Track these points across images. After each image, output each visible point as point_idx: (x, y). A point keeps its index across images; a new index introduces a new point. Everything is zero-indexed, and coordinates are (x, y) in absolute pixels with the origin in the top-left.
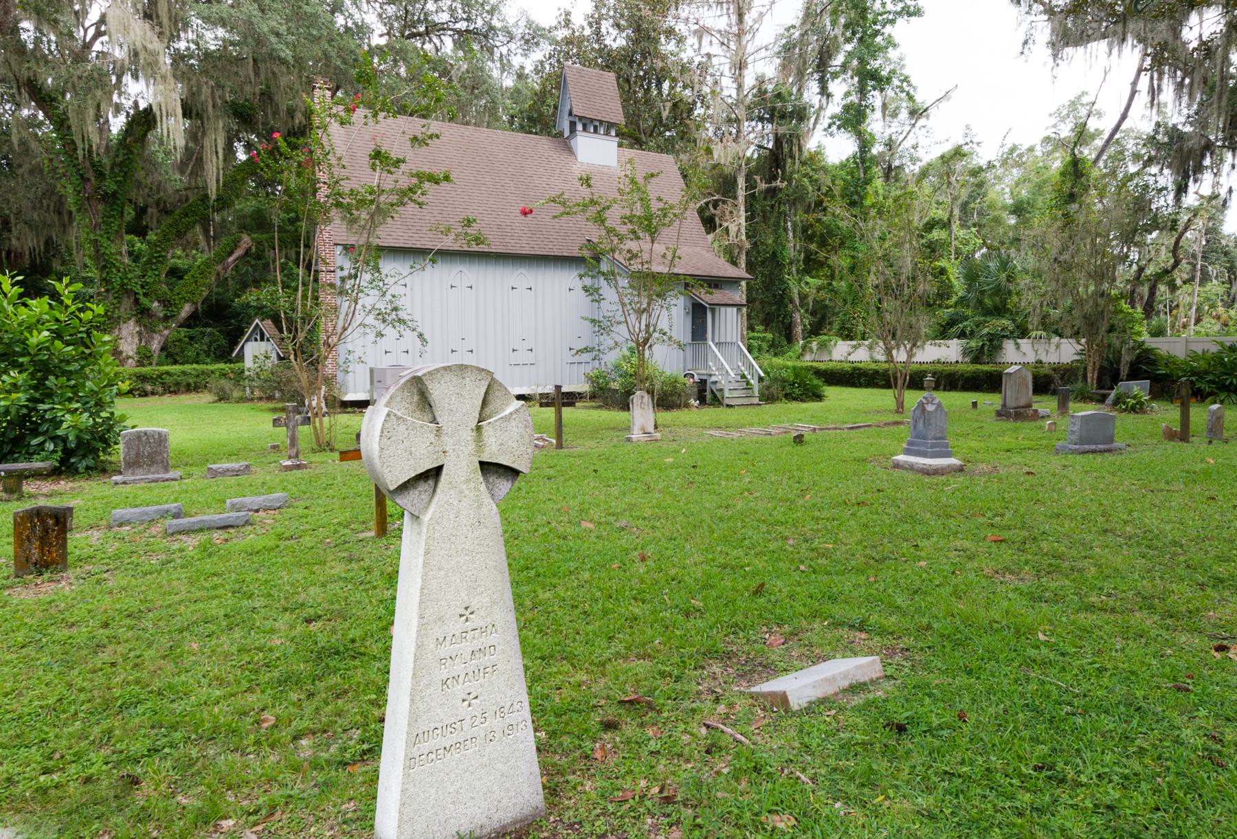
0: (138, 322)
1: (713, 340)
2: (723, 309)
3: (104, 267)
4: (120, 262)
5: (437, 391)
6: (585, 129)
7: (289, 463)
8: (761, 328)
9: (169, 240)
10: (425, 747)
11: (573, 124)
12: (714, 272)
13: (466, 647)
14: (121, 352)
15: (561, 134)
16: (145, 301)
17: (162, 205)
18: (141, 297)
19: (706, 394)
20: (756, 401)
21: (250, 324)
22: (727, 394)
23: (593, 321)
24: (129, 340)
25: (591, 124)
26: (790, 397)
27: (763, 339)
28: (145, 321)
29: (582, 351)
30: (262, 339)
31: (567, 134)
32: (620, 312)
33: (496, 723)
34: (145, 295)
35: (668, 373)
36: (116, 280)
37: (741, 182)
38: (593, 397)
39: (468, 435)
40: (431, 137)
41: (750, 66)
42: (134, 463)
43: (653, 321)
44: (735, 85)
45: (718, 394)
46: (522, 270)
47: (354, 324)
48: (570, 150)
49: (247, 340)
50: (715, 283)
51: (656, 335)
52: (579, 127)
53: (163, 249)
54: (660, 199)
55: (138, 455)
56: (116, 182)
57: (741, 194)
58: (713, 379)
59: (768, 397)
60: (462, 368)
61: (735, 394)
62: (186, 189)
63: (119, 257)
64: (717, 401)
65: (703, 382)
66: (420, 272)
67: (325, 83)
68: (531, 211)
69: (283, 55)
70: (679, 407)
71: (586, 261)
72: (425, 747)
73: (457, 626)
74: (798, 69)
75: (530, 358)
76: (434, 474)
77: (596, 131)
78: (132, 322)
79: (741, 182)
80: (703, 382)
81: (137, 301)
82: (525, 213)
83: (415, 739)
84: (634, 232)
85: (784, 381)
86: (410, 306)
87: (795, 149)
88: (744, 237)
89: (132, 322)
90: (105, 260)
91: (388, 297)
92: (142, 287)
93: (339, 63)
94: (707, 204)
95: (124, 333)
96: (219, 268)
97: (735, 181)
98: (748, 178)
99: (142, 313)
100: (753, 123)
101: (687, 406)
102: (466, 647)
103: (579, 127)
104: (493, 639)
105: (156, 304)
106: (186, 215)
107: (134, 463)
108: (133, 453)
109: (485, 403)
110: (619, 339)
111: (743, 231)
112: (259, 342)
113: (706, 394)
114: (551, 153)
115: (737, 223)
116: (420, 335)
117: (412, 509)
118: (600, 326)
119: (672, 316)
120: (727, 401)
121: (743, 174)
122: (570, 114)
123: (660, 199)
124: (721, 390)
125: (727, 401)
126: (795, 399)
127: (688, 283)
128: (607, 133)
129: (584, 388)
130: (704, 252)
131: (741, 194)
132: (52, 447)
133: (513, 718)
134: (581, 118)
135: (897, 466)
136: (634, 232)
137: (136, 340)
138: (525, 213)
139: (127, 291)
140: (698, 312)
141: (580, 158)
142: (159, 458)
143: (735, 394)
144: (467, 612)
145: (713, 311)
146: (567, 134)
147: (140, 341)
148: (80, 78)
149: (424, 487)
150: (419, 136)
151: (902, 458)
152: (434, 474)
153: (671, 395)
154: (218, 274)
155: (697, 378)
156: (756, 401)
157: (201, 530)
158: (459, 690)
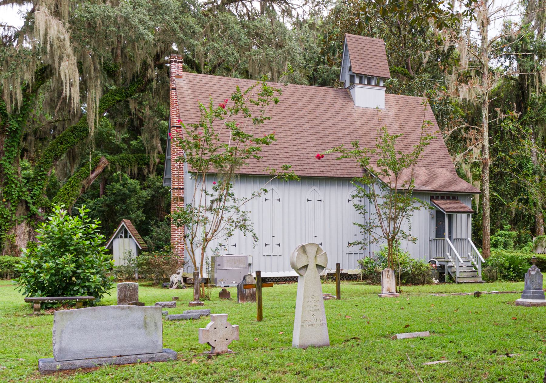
0: (28, 224)
1: (450, 238)
2: (455, 214)
3: (6, 183)
4: (17, 179)
5: (308, 249)
6: (361, 83)
7: (195, 302)
8: (509, 227)
9: (49, 162)
10: (305, 323)
11: (352, 77)
12: (453, 188)
13: (313, 304)
14: (16, 246)
15: (343, 84)
16: (33, 208)
17: (38, 134)
18: (31, 206)
19: (444, 275)
20: (480, 280)
21: (118, 226)
22: (458, 275)
23: (360, 225)
24: (22, 237)
25: (367, 79)
26: (506, 278)
27: (509, 236)
28: (33, 223)
29: (354, 244)
30: (126, 237)
31: (347, 84)
32: (377, 220)
33: (319, 322)
34: (34, 203)
35: (416, 260)
36: (15, 194)
37: (485, 113)
38: (365, 277)
39: (314, 258)
40: (265, 119)
41: (492, 23)
42: (123, 300)
43: (397, 225)
44: (480, 37)
45: (453, 276)
46: (314, 188)
47: (220, 229)
48: (349, 98)
49: (115, 238)
50: (452, 196)
51: (399, 234)
52: (357, 81)
53: (45, 169)
54: (400, 153)
55: (125, 295)
56: (17, 121)
57: (485, 123)
58: (450, 264)
59: (490, 278)
60: (312, 244)
61: (465, 275)
62: (56, 121)
63: (16, 176)
64: (452, 280)
65: (443, 267)
66: (258, 197)
67: (179, 58)
68: (323, 156)
69: (147, 38)
70: (423, 283)
71: (363, 180)
72: (305, 323)
73: (311, 299)
74: (538, 16)
75: (278, 250)
76: (306, 266)
77: (369, 84)
78: (24, 224)
79: (485, 113)
80: (443, 267)
81: (28, 208)
82: (319, 157)
83: (303, 321)
84: (385, 171)
85: (502, 265)
86: (255, 221)
87: (536, 80)
88: (487, 156)
89: (24, 224)
90: (7, 178)
91: (241, 213)
92: (32, 198)
93: (181, 35)
94: (460, 130)
95: (19, 232)
96: (84, 182)
97: (481, 112)
98: (492, 110)
99: (31, 217)
100: (502, 59)
101: (429, 283)
102: (313, 304)
103: (357, 81)
104: (318, 304)
105: (40, 210)
106: (62, 143)
107: (123, 300)
108: (123, 294)
109: (317, 252)
110: (377, 237)
111: (487, 151)
112: (123, 239)
113: (444, 275)
114: (336, 100)
115: (480, 146)
116: (254, 235)
117: (419, 131)
118: (367, 229)
119: (418, 221)
120: (458, 280)
121: (487, 107)
122: (350, 70)
123: (400, 153)
124: (454, 272)
125: (458, 280)
126: (510, 280)
127: (434, 195)
128: (378, 85)
129: (358, 271)
130: (448, 172)
131: (485, 123)
132: (83, 291)
133: (323, 322)
134: (358, 75)
135: (518, 304)
136: (385, 171)
137: (27, 238)
138: (319, 157)
139: (21, 201)
140: (439, 216)
141: (357, 104)
142: (134, 297)
143: (465, 275)
144: (313, 297)
145: (450, 218)
146: (347, 84)
147: (30, 237)
148: (11, 56)
149: (304, 269)
150: (258, 118)
151: (520, 300)
152: (306, 266)
153: (418, 275)
154: (84, 187)
155: (438, 264)
156: (480, 280)
157: (182, 320)
158: (312, 313)
